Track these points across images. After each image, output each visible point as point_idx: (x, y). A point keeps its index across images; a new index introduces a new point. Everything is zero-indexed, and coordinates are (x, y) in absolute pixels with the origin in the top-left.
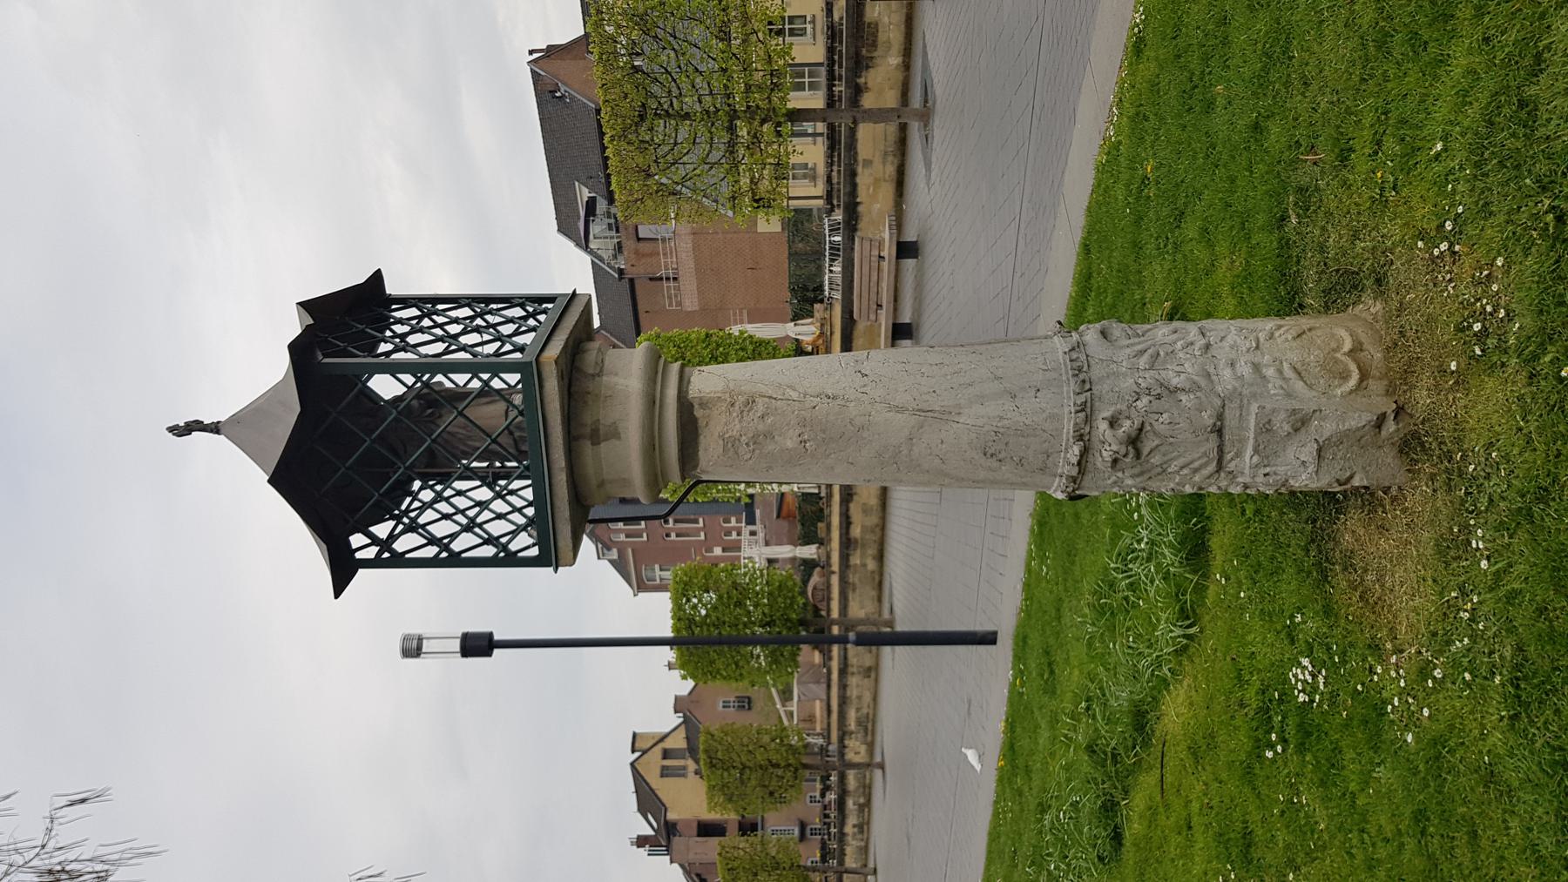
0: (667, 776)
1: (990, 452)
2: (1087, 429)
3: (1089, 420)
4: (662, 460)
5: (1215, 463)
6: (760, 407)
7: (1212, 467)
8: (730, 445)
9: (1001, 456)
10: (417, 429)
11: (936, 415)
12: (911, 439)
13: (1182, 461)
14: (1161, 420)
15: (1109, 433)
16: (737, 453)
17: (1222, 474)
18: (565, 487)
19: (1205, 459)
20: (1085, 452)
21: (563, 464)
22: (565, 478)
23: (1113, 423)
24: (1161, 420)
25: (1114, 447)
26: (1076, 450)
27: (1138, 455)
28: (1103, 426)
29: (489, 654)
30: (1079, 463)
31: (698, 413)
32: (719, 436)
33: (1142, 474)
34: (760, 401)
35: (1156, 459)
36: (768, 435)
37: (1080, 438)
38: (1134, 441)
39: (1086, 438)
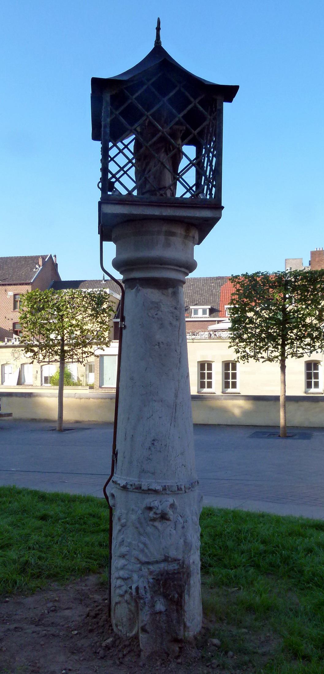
0: (300, 259)
1: (156, 443)
2: (168, 492)
3: (173, 493)
4: (156, 268)
5: (147, 560)
6: (175, 323)
7: (144, 559)
8: (156, 305)
9: (152, 449)
10: (155, 139)
11: (174, 413)
12: (162, 401)
13: (148, 542)
14: (172, 530)
15: (168, 504)
16: (151, 309)
17: (139, 565)
18: (151, 213)
19: (149, 555)
20: (156, 492)
21: (164, 214)
22: (156, 214)
23: (172, 506)
24: (172, 530)
25: (160, 507)
26: (159, 488)
27: (154, 520)
28: (171, 500)
29: (96, 136)
30: (149, 490)
31: (170, 290)
32: (161, 300)
33: (141, 523)
34: (178, 323)
35: (149, 529)
36: (162, 326)
37: (164, 489)
38: (164, 517)
39: (163, 492)
